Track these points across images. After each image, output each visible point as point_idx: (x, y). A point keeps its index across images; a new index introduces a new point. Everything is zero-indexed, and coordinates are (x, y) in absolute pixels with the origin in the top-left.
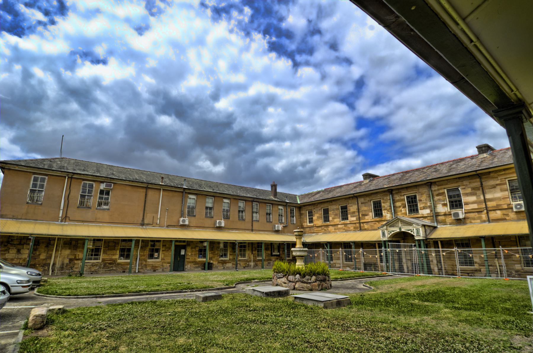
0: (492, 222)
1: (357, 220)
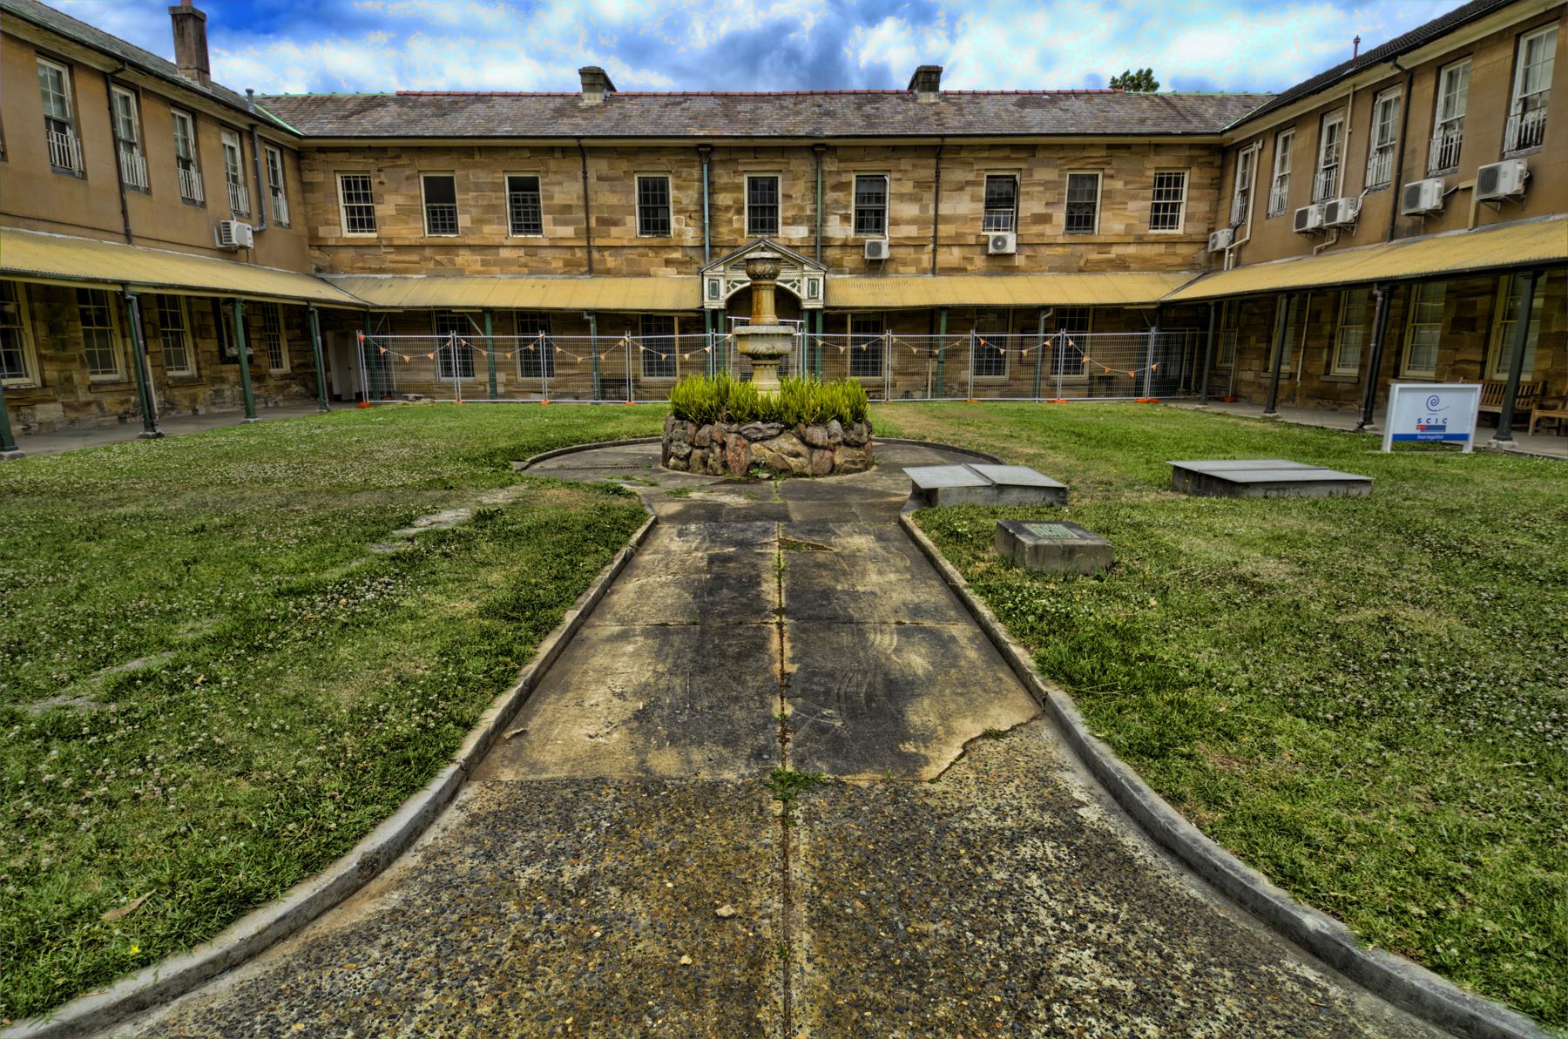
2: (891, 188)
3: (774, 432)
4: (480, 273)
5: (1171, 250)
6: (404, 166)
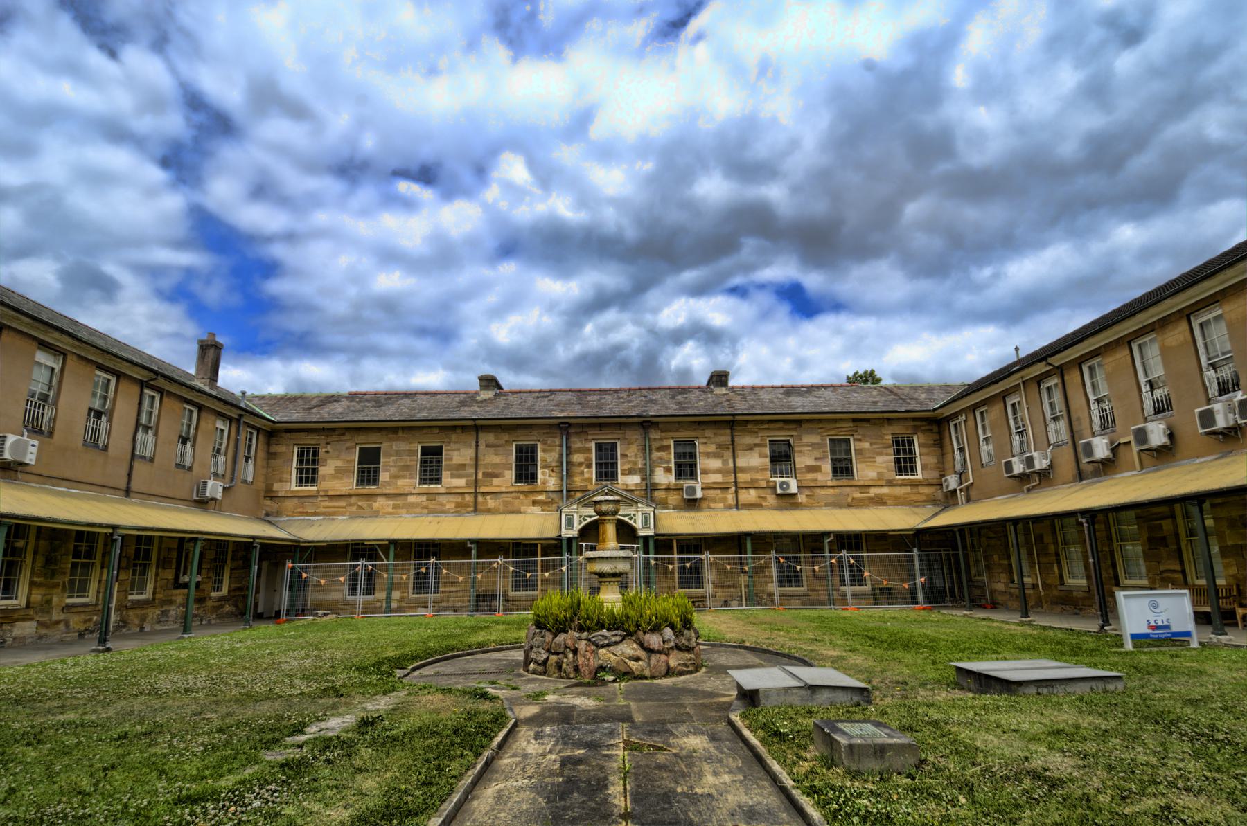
1: (468, 485)
2: (699, 449)
3: (617, 639)
4: (391, 514)
5: (915, 490)
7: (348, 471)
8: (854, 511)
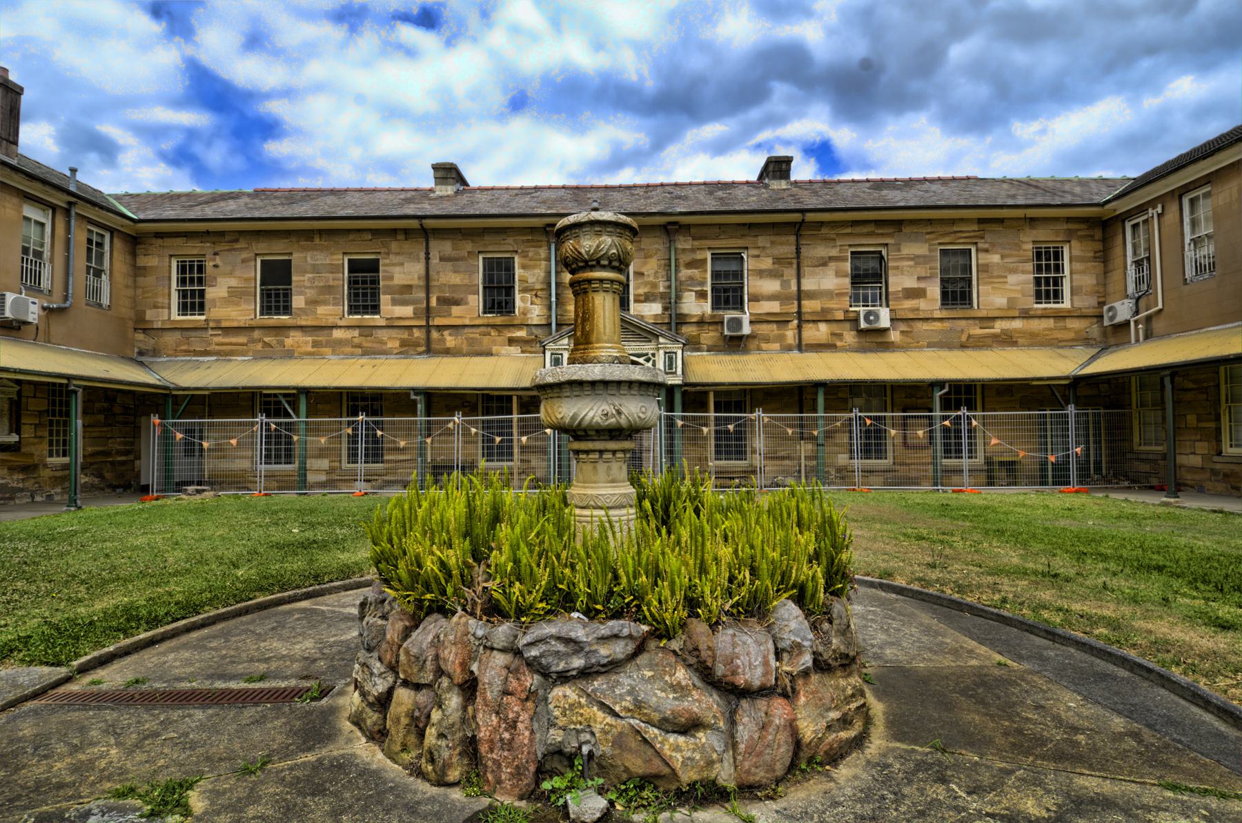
0: (806, 351)
2: (749, 264)
3: (619, 649)
4: (310, 354)
5: (1061, 324)
6: (241, 249)
7: (248, 294)
8: (970, 352)
